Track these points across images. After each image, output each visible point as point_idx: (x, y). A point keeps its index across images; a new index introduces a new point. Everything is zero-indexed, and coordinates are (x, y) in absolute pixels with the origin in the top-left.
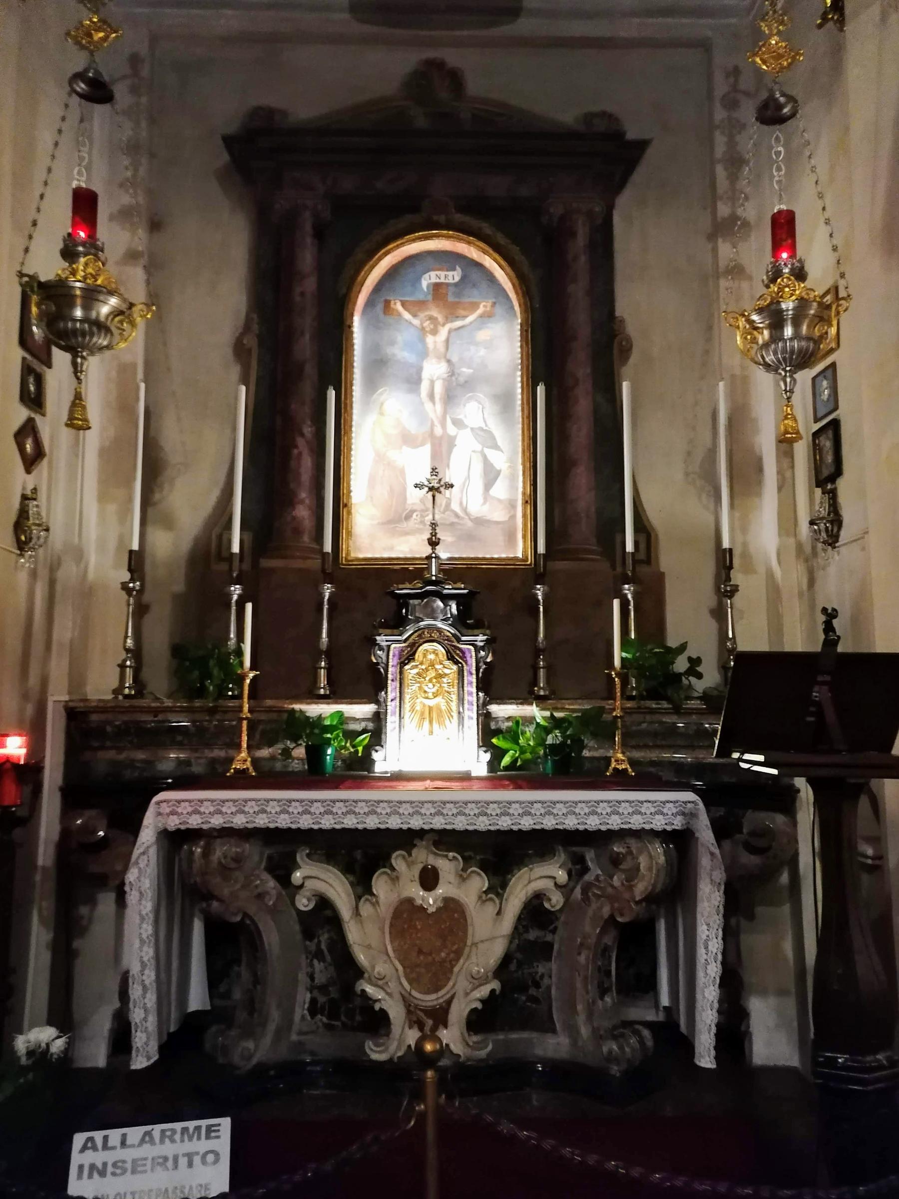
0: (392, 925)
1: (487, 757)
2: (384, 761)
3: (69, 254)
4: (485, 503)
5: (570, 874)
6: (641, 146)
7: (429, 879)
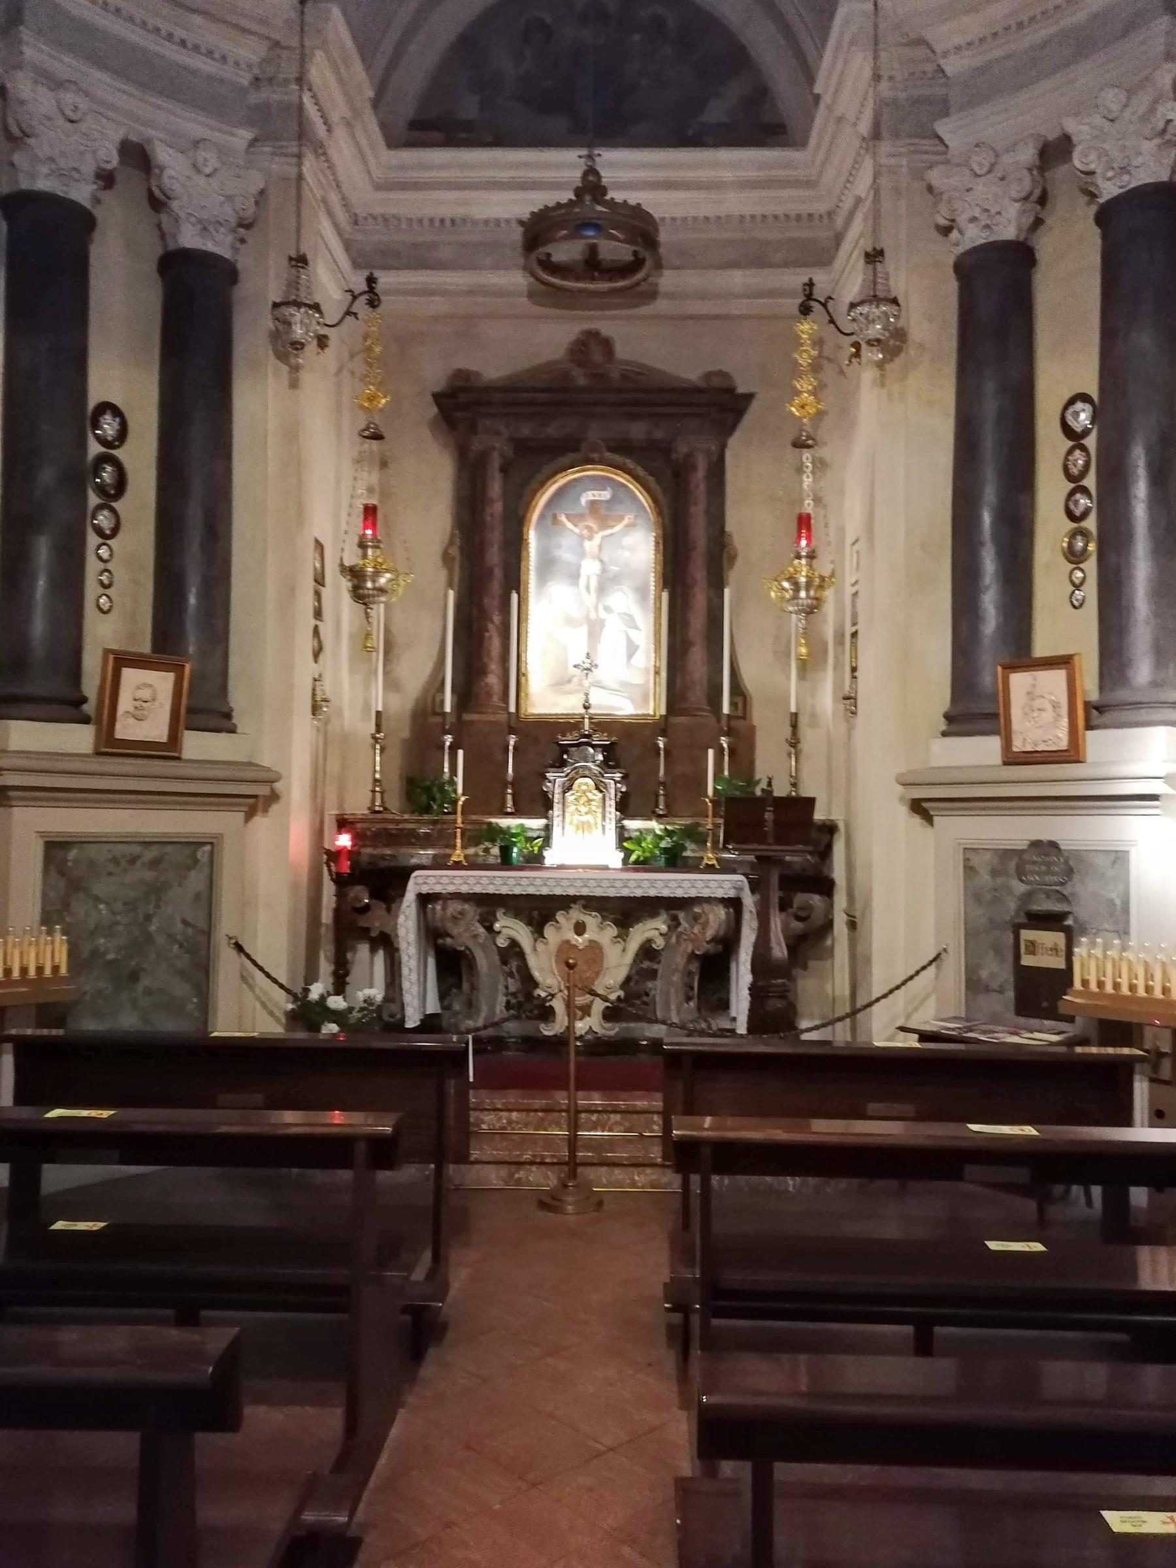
0: (557, 956)
1: (622, 855)
2: (551, 857)
5: (669, 927)
6: (749, 397)
7: (580, 929)
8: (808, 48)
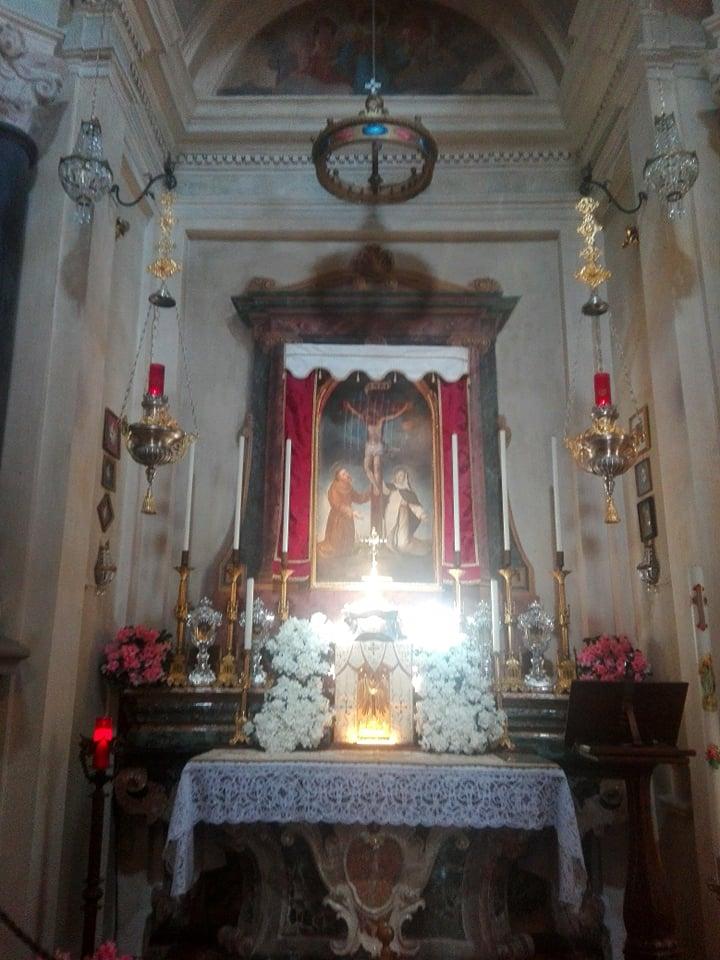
3: (147, 405)
4: (409, 542)
6: (515, 300)
8: (107, 455)
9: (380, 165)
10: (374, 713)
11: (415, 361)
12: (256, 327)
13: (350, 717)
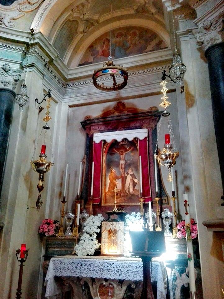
3: (41, 157)
4: (133, 191)
9: (116, 79)
10: (113, 245)
11: (130, 135)
12: (87, 130)
13: (106, 246)
